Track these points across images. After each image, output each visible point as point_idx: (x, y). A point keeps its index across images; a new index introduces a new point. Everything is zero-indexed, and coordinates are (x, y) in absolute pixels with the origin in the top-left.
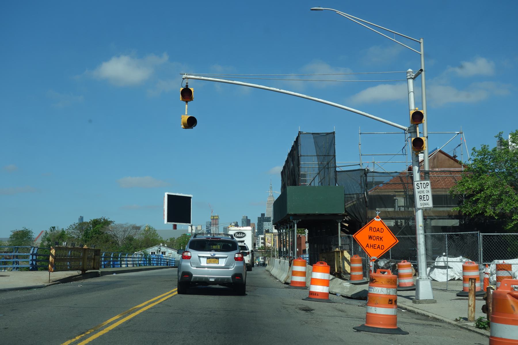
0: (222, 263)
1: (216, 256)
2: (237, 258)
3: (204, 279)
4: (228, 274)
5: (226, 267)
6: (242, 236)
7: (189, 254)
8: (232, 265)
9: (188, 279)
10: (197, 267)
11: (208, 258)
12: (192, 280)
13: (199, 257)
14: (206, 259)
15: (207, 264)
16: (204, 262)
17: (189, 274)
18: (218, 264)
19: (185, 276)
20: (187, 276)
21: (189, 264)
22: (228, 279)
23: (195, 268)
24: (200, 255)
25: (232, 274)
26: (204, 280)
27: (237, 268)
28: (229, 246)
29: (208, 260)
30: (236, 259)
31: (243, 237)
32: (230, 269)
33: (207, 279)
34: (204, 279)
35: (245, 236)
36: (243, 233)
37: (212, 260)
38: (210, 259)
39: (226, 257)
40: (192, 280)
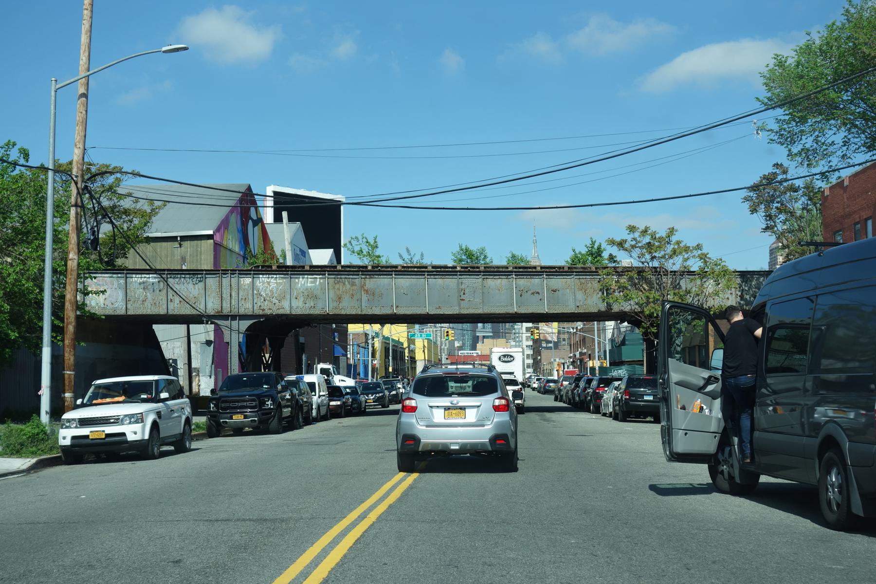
0: (471, 416)
1: (460, 404)
2: (499, 405)
3: (480, 445)
4: (482, 435)
5: (479, 424)
6: (509, 360)
7: (413, 403)
8: (490, 420)
9: (412, 446)
10: (427, 426)
11: (447, 409)
12: (420, 449)
13: (431, 407)
14: (443, 410)
15: (445, 419)
16: (439, 416)
17: (415, 439)
18: (465, 418)
19: (407, 443)
20: (412, 443)
21: (414, 421)
22: (483, 444)
23: (425, 428)
24: (431, 404)
25: (490, 434)
26: (440, 448)
27: (499, 425)
28: (267, 385)
29: (446, 412)
30: (497, 408)
31: (511, 361)
32: (486, 427)
33: (446, 445)
34: (480, 445)
35: (513, 359)
36: (511, 356)
37: (454, 412)
38: (450, 411)
39: (478, 406)
40: (420, 449)
